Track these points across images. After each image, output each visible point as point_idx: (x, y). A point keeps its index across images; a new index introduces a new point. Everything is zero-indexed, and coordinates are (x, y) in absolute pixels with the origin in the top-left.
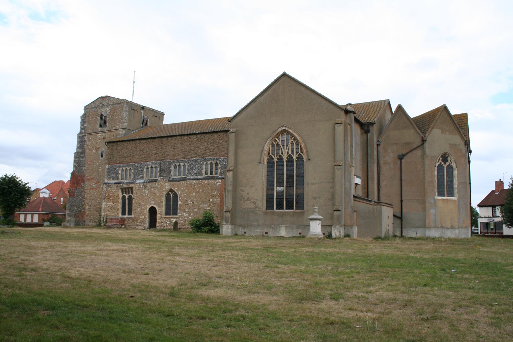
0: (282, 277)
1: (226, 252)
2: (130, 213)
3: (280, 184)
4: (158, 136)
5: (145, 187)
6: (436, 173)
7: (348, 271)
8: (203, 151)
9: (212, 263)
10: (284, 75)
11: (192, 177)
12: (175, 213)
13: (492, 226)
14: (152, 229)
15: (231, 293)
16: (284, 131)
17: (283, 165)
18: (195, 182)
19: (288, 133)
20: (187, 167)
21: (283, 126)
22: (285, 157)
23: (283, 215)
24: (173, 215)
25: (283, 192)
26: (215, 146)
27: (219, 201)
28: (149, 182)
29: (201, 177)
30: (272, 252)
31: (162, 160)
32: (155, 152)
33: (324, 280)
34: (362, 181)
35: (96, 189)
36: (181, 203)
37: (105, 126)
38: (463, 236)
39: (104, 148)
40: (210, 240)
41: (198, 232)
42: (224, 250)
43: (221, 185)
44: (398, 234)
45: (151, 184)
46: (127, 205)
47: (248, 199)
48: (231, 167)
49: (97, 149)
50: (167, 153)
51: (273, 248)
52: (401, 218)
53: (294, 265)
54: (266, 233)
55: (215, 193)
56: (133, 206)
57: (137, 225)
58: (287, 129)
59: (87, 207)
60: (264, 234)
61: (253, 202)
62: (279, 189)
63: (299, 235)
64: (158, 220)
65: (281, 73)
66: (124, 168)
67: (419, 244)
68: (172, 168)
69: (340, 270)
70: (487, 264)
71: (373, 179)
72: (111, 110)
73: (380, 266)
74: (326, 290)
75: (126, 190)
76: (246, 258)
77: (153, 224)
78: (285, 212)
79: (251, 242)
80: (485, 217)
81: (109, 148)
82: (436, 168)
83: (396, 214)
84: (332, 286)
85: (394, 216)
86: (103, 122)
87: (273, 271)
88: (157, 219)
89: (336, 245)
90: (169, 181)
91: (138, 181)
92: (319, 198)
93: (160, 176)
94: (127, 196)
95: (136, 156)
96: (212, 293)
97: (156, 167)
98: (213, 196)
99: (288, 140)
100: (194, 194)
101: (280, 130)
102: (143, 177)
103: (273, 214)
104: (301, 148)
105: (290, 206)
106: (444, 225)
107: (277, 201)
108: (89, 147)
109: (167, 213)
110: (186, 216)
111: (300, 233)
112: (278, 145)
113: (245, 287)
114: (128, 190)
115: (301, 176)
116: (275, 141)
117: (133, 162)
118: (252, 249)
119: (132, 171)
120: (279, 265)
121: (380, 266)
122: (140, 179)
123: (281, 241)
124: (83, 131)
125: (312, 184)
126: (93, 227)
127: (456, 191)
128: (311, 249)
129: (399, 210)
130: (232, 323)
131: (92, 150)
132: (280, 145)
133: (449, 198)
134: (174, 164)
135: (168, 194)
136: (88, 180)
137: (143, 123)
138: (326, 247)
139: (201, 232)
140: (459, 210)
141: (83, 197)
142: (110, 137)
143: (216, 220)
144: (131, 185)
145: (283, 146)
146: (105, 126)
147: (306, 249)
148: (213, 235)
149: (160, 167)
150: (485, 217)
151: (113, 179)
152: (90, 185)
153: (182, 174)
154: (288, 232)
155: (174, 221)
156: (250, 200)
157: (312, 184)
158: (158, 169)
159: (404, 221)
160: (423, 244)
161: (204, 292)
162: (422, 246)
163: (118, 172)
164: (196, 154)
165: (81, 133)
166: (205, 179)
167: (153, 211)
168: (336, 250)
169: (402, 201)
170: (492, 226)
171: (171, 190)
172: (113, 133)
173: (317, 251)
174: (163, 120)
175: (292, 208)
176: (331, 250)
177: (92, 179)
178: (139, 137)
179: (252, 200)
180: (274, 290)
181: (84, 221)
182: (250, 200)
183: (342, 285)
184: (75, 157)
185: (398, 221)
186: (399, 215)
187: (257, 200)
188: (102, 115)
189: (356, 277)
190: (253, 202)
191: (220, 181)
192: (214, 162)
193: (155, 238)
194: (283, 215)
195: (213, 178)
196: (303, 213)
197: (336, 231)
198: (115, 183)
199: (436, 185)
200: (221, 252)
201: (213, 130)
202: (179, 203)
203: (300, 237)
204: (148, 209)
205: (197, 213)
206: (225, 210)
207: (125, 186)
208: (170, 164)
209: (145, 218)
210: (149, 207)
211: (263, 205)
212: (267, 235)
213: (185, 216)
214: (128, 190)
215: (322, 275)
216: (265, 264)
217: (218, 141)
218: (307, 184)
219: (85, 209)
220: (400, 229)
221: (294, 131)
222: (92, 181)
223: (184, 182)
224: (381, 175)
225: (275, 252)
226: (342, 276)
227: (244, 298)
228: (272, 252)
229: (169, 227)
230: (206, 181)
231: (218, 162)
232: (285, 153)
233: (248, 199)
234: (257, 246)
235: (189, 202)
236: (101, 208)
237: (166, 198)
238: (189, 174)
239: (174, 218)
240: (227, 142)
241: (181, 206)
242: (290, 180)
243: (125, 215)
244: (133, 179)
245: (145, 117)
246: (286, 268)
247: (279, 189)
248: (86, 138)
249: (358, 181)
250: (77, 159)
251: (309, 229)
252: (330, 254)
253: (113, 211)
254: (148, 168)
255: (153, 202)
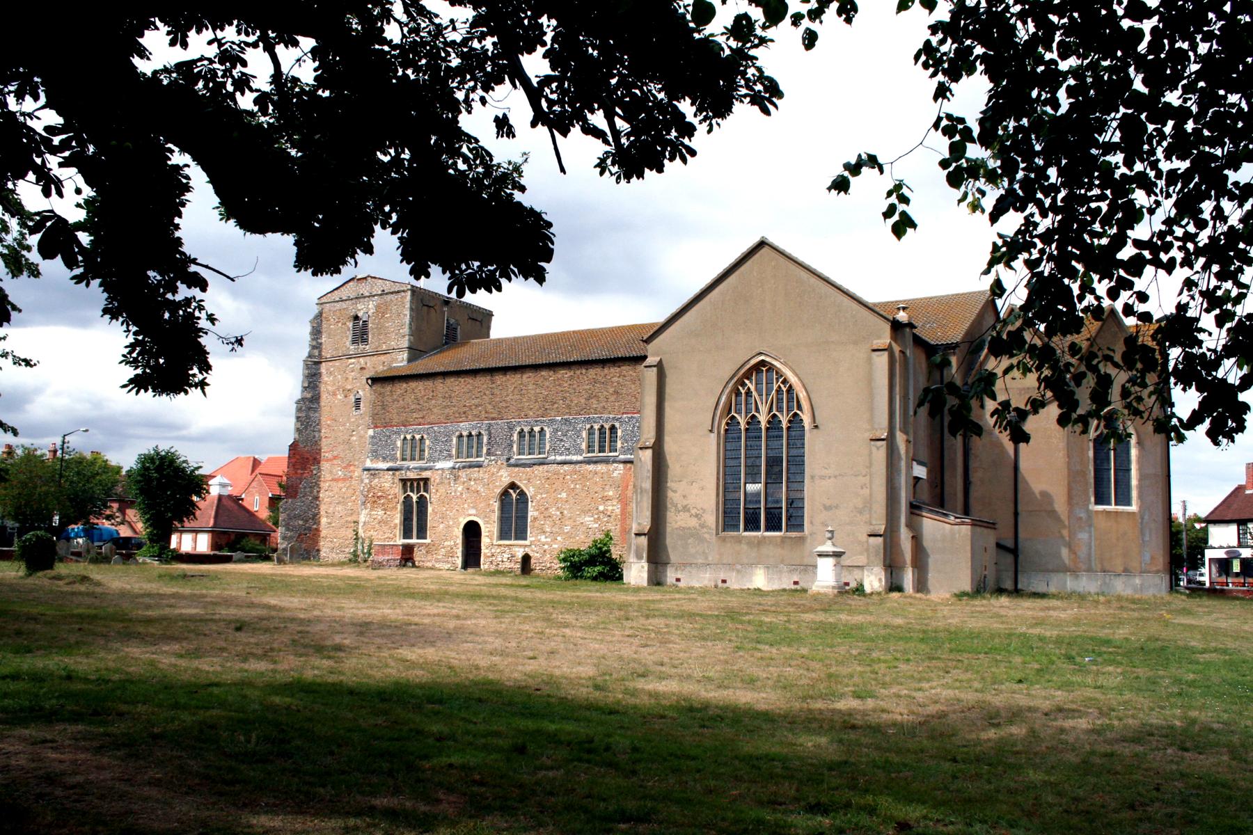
0: (768, 666)
1: (651, 620)
2: (422, 533)
3: (753, 476)
4: (482, 366)
5: (456, 478)
6: (1091, 454)
7: (889, 657)
8: (583, 401)
9: (636, 641)
10: (762, 244)
11: (559, 458)
12: (521, 534)
13: (1236, 567)
14: (470, 570)
15: (689, 688)
16: (763, 363)
17: (760, 437)
18: (566, 467)
19: (771, 368)
20: (548, 436)
21: (761, 354)
22: (763, 418)
23: (761, 542)
24: (516, 539)
25: (758, 494)
26: (611, 390)
27: (618, 511)
28: (464, 467)
29: (580, 458)
30: (742, 622)
31: (493, 419)
32: (476, 401)
33: (844, 671)
34: (929, 473)
35: (344, 480)
36: (536, 514)
37: (365, 341)
38: (1149, 594)
39: (365, 392)
40: (607, 595)
41: (576, 577)
42: (647, 617)
43: (623, 477)
44: (1008, 585)
45: (469, 471)
46: (415, 518)
47: (686, 509)
48: (647, 440)
49: (347, 392)
50: (504, 404)
51: (743, 614)
52: (1014, 551)
53: (789, 645)
54: (724, 581)
55: (611, 493)
56: (429, 518)
57: (437, 561)
58: (768, 359)
59: (324, 521)
60: (720, 584)
61: (697, 516)
62: (751, 488)
63: (793, 587)
64: (484, 550)
65: (754, 240)
66: (409, 437)
67: (1048, 609)
68: (515, 437)
69: (875, 655)
70: (1163, 649)
71: (954, 469)
72: (378, 307)
73: (951, 651)
74: (847, 685)
75: (412, 485)
76: (696, 634)
77: (472, 555)
78: (764, 538)
79: (695, 600)
80: (1221, 547)
81: (375, 391)
82: (1091, 444)
83: (1002, 542)
84: (856, 679)
85: (999, 546)
86: (361, 334)
87: (752, 656)
88: (483, 548)
89: (871, 609)
90: (509, 466)
91: (439, 465)
92: (837, 507)
93: (488, 454)
94: (415, 497)
95: (435, 410)
96: (651, 686)
97: (479, 435)
98: (606, 499)
99: (769, 383)
100: (564, 495)
101: (753, 362)
102: (450, 456)
103: (739, 540)
104: (798, 402)
105: (774, 524)
106: (1108, 567)
107: (746, 513)
108: (330, 388)
109: (504, 534)
110: (547, 543)
111: (796, 583)
112: (748, 393)
113: (709, 679)
114: (418, 485)
115: (797, 462)
116: (743, 385)
117: (429, 423)
118: (701, 615)
119: (427, 442)
120: (759, 646)
121: (951, 651)
122: (445, 459)
123: (757, 599)
124: (316, 352)
125: (822, 478)
126: (341, 564)
127: (1134, 494)
128: (820, 617)
129: (1011, 535)
130: (707, 723)
131: (334, 394)
132: (755, 394)
133: (1120, 508)
134: (518, 429)
135: (505, 494)
136: (327, 460)
137: (447, 335)
138: (851, 612)
139: (581, 577)
140: (1142, 533)
141: (317, 498)
142: (378, 366)
143: (615, 553)
144: (425, 474)
145: (760, 395)
146: (365, 341)
147: (808, 617)
148: (609, 584)
149: (490, 434)
150: (1221, 547)
151: (384, 459)
152: (331, 472)
153: (536, 451)
154: (770, 580)
155: (520, 553)
156: (688, 511)
157: (822, 478)
158: (485, 439)
159: (1021, 557)
160: (1054, 609)
161: (641, 684)
162: (1051, 613)
163: (395, 444)
164: (569, 407)
165: (310, 356)
166: (589, 462)
167: (472, 532)
168: (869, 618)
169: (1016, 514)
170: (1236, 567)
171: (513, 486)
172: (382, 358)
173: (831, 620)
174: (489, 328)
175: (780, 529)
176: (859, 619)
177: (335, 458)
178: (442, 369)
179: (693, 512)
180: (759, 684)
181: (318, 551)
182: (688, 511)
183: (875, 679)
184: (299, 410)
185: (1009, 558)
186: (1010, 543)
187: (704, 511)
188: (356, 318)
189: (903, 667)
190: (697, 516)
191: (621, 466)
192: (607, 426)
193: (494, 592)
194: (761, 542)
195: (606, 461)
196: (802, 539)
197: (872, 577)
198: (388, 470)
199: (1092, 481)
200: (642, 621)
201: (604, 354)
202: (530, 514)
203: (796, 591)
204: (462, 526)
205: (569, 536)
206: (634, 531)
207: (411, 475)
208: (511, 429)
209: (456, 545)
210: (463, 521)
211: (711, 519)
212: (725, 585)
213: (547, 543)
214: (418, 485)
215: (840, 663)
216: (734, 644)
217: (616, 379)
218: (812, 477)
219: (319, 523)
220: (1011, 574)
221: (785, 364)
222: (335, 462)
223: (541, 468)
224: (972, 458)
225: (749, 622)
226: (876, 667)
227: (712, 694)
228: (742, 622)
229: (508, 565)
230: (591, 467)
231: (617, 425)
232: (764, 409)
233: (686, 509)
234: (710, 608)
235: (553, 511)
236: (356, 522)
237: (502, 501)
238: (554, 450)
239: (521, 546)
240: (639, 381)
241: (493, 511)
242: (776, 469)
243: (411, 537)
244: (429, 461)
245: (452, 321)
246: (774, 651)
247: (751, 488)
248: (324, 368)
249: (920, 471)
250: (303, 414)
251: (815, 574)
252: (859, 627)
253: (385, 528)
254: (461, 436)
255: (473, 512)
